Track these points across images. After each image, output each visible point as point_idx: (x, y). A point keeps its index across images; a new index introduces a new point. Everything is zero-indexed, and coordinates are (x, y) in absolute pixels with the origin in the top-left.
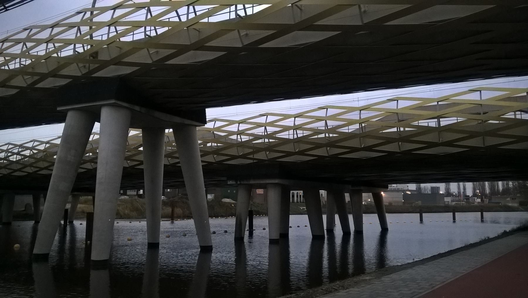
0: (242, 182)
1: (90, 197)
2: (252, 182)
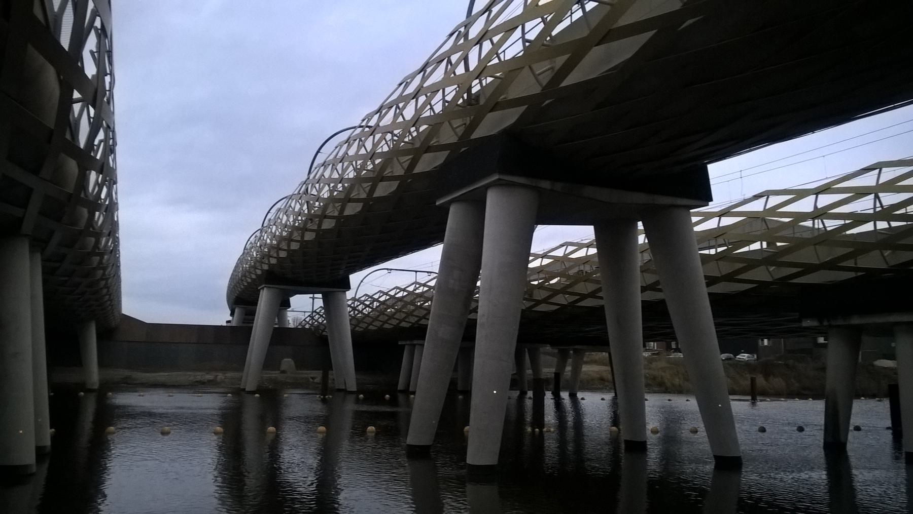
0: (833, 323)
1: (605, 355)
2: (856, 321)
